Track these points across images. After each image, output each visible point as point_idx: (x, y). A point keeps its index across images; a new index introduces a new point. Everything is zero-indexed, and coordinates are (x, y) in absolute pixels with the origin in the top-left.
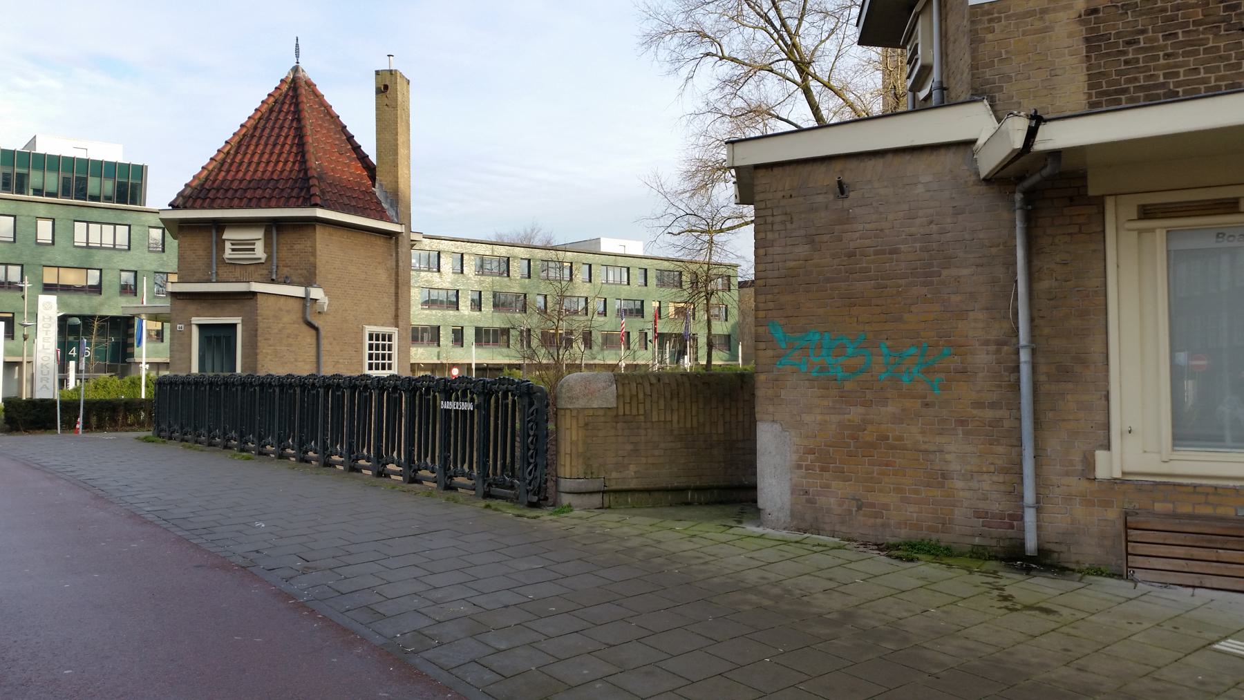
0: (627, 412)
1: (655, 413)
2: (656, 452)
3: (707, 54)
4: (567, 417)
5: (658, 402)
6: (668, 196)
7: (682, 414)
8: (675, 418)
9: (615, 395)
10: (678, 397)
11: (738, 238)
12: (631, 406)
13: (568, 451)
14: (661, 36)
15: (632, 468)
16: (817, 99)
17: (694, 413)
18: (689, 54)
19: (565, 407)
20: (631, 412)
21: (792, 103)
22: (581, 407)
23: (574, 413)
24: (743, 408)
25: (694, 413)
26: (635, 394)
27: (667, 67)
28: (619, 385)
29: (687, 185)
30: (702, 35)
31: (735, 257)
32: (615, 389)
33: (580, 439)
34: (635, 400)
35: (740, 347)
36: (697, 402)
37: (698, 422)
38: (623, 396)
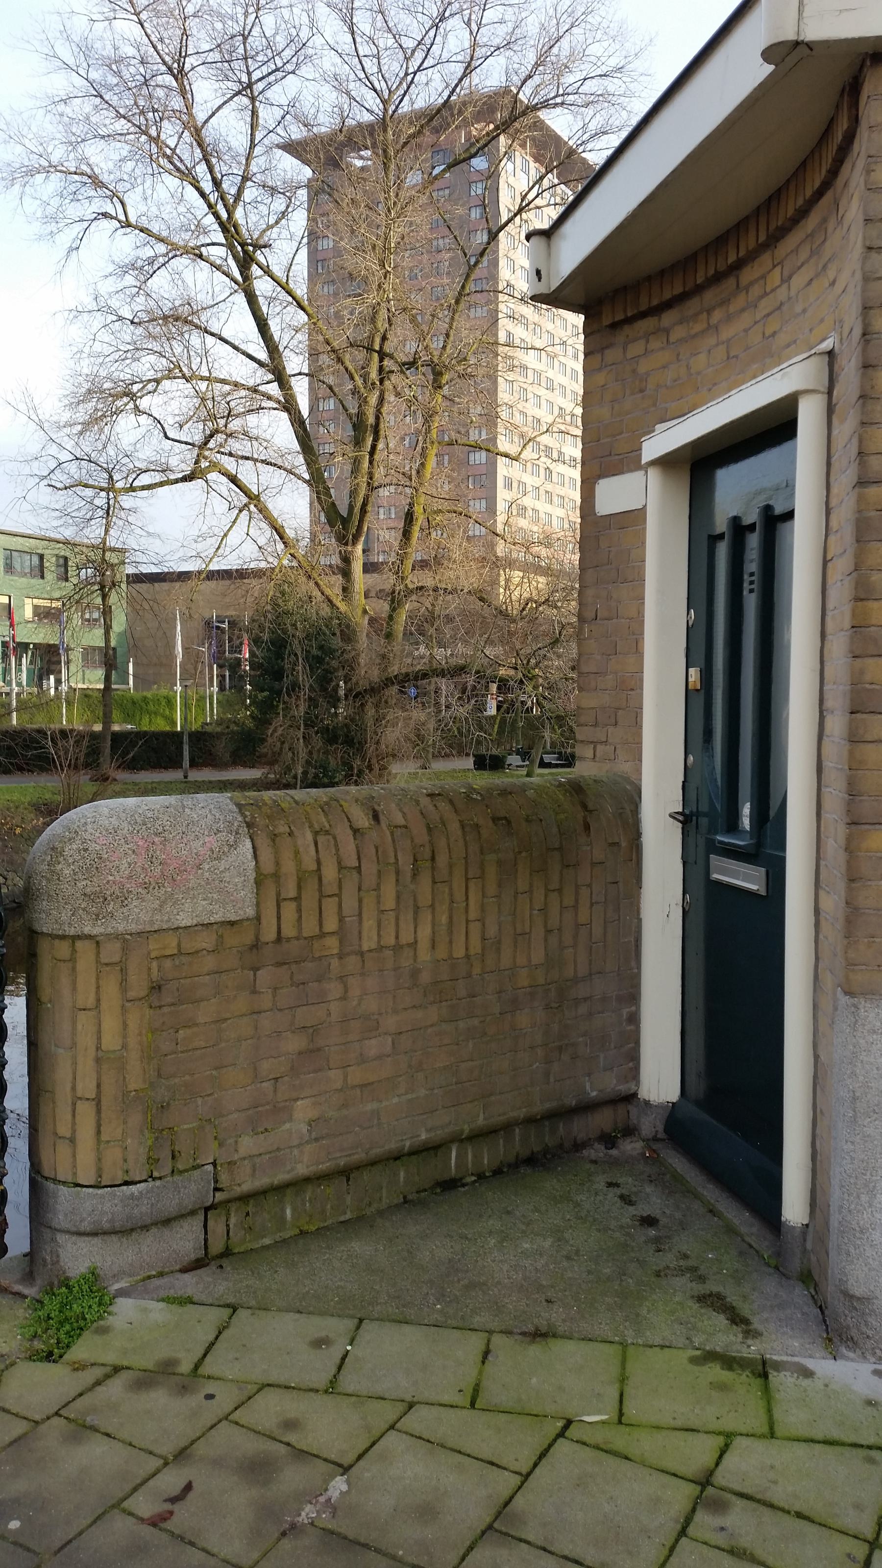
0: (289, 931)
1: (369, 924)
2: (373, 1047)
3: (105, 215)
4: (81, 965)
5: (378, 888)
6: (46, 425)
7: (444, 919)
8: (425, 932)
9: (252, 875)
10: (433, 868)
11: (150, 505)
12: (299, 910)
13: (87, 1087)
14: (31, 172)
15: (303, 1111)
16: (265, 309)
17: (473, 914)
18: (74, 211)
19: (72, 932)
20: (300, 929)
21: (228, 310)
22: (133, 927)
23: (112, 952)
24: (589, 886)
25: (473, 914)
26: (314, 867)
27: (36, 227)
28: (263, 842)
29: (82, 414)
30: (97, 182)
31: (144, 534)
32: (249, 855)
33: (132, 1041)
34: (311, 886)
35: (131, 665)
36: (482, 877)
37: (484, 939)
38: (276, 876)
